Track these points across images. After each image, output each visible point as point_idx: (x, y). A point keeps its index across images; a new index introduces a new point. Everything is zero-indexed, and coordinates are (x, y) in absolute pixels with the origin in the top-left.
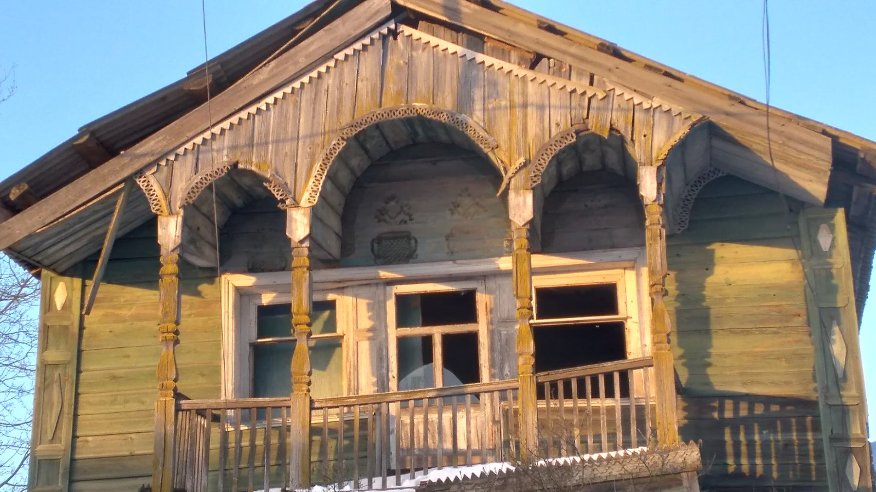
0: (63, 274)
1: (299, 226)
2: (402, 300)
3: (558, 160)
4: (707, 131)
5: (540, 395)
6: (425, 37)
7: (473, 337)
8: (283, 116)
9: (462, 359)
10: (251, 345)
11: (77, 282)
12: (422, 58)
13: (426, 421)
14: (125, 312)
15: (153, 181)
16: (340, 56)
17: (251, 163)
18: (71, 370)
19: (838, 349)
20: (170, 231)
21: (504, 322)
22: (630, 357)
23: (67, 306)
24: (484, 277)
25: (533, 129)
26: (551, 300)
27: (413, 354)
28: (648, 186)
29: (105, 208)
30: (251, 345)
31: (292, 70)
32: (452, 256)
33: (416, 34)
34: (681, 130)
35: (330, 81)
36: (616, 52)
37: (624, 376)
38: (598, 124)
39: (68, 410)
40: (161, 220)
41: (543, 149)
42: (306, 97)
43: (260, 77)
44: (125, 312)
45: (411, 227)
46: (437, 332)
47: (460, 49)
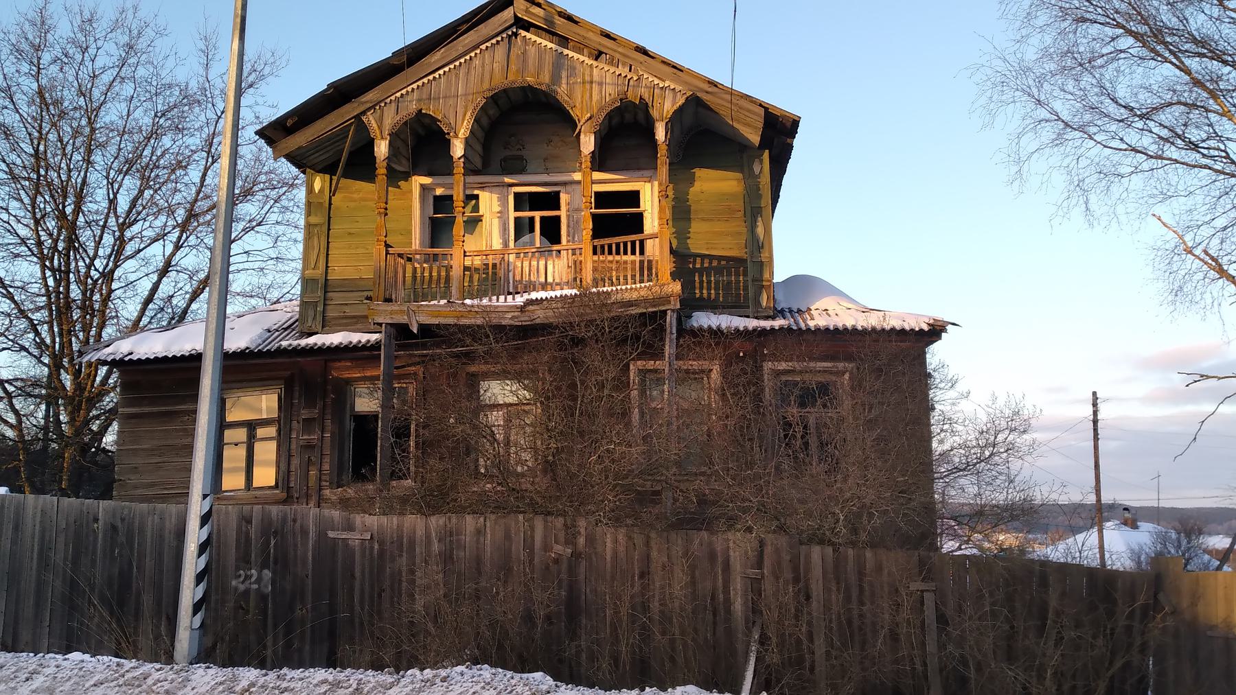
0: (319, 172)
2: (517, 195)
3: (609, 116)
5: (595, 253)
7: (558, 218)
9: (551, 231)
11: (327, 177)
12: (532, 50)
14: (355, 196)
19: (760, 230)
20: (382, 149)
21: (576, 209)
24: (565, 184)
25: (595, 97)
26: (603, 199)
27: (523, 227)
28: (660, 134)
31: (455, 55)
32: (547, 171)
33: (528, 35)
34: (681, 101)
35: (477, 62)
36: (644, 51)
39: (323, 251)
41: (601, 109)
43: (436, 57)
44: (355, 196)
45: (523, 153)
46: (537, 215)
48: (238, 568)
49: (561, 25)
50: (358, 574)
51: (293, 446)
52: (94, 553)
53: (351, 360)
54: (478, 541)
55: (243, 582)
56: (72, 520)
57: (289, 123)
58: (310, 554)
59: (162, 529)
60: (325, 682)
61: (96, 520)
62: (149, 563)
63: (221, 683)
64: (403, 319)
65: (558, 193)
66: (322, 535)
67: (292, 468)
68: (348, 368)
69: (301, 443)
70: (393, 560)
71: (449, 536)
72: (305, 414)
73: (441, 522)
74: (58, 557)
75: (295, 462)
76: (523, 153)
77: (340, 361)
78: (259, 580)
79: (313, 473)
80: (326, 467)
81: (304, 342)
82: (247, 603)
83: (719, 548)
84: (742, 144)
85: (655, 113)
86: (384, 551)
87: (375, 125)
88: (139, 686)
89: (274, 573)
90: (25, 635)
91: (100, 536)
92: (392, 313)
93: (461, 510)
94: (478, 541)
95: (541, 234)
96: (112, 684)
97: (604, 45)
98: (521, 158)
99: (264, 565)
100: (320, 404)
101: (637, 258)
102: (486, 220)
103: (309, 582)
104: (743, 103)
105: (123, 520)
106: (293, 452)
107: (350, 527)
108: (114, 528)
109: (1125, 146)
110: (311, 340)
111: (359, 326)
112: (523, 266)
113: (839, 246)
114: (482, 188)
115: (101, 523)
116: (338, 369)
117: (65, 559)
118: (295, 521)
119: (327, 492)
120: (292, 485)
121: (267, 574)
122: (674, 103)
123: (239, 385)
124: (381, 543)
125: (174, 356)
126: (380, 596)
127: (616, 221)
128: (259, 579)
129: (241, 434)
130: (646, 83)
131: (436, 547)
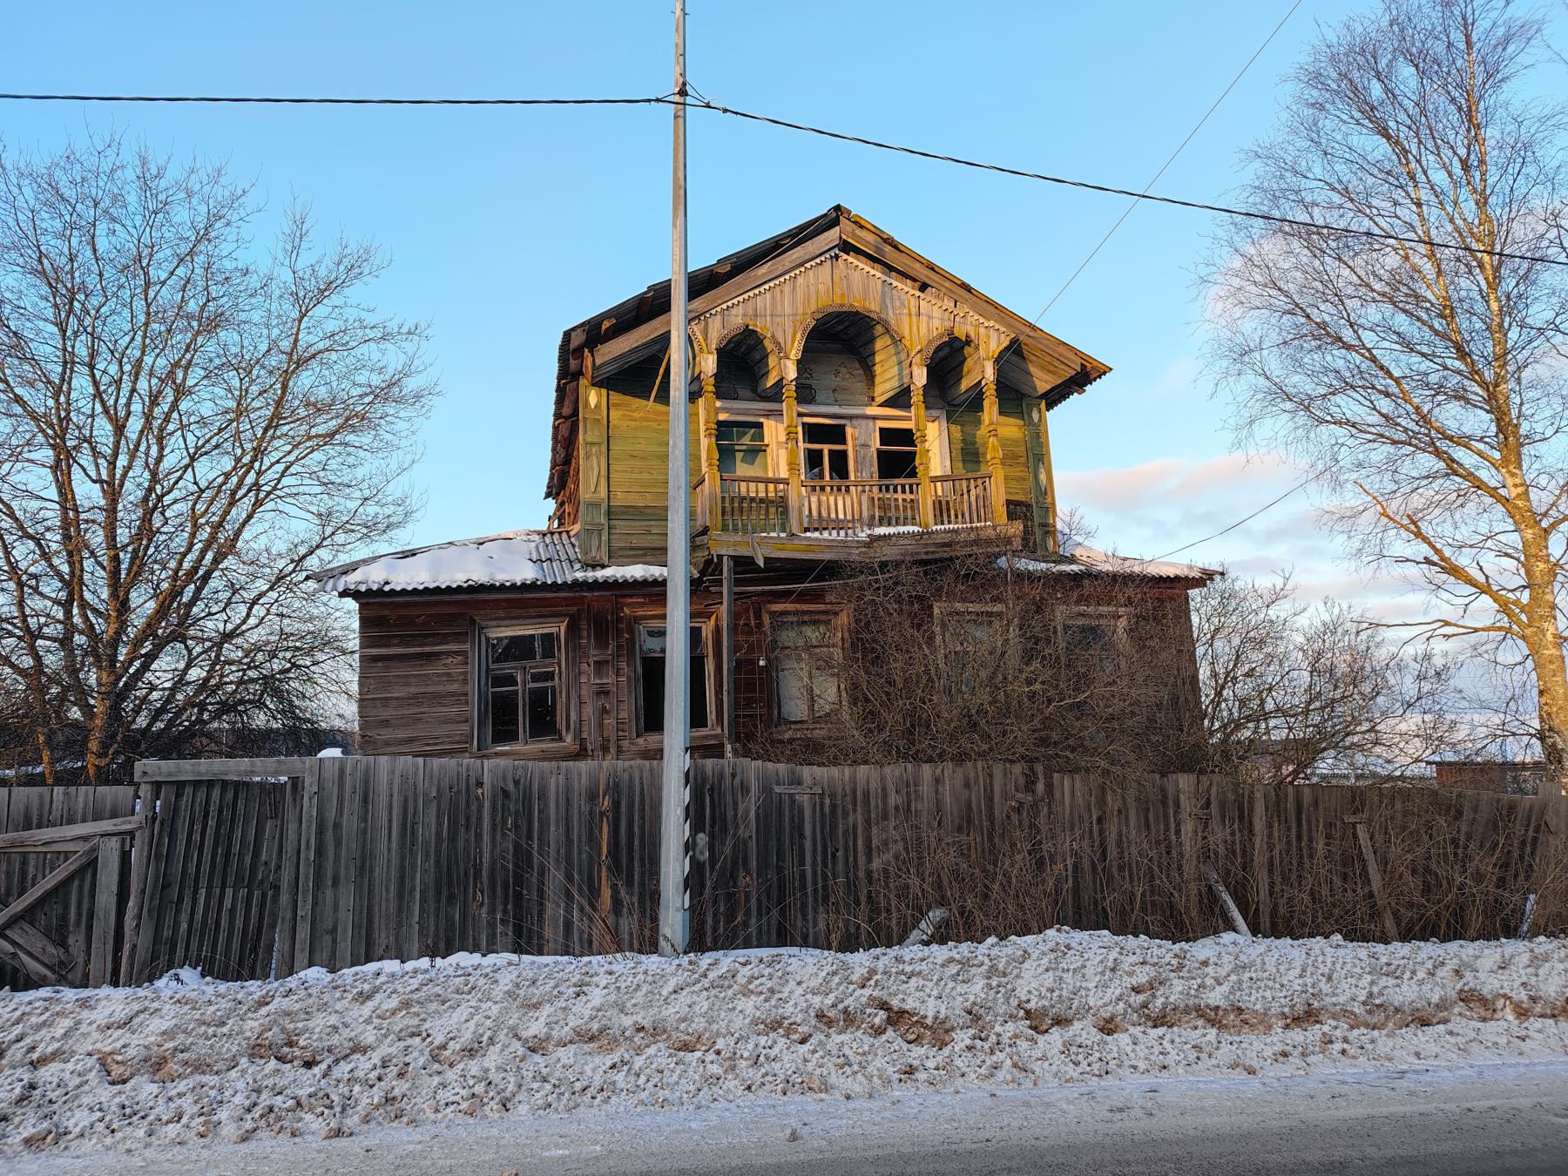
3: (938, 349)
7: (844, 453)
8: (773, 297)
9: (840, 465)
11: (604, 392)
12: (856, 275)
13: (819, 502)
14: (636, 415)
17: (758, 326)
18: (604, 448)
19: (1043, 477)
21: (862, 442)
23: (598, 406)
24: (851, 418)
25: (923, 330)
26: (887, 436)
27: (814, 459)
32: (836, 402)
33: (850, 259)
35: (800, 280)
36: (967, 288)
38: (960, 332)
42: (787, 288)
43: (763, 271)
44: (636, 415)
46: (826, 448)
47: (879, 274)
49: (890, 255)
50: (808, 832)
53: (644, 596)
54: (937, 792)
56: (445, 785)
57: (606, 324)
58: (752, 813)
59: (568, 790)
60: (951, 960)
61: (480, 784)
63: (835, 973)
64: (744, 551)
65: (843, 427)
66: (766, 790)
68: (641, 605)
70: (845, 815)
71: (909, 788)
73: (897, 773)
74: (427, 828)
77: (631, 596)
81: (591, 575)
83: (1171, 789)
86: (832, 808)
88: (730, 987)
89: (712, 836)
90: (382, 938)
91: (487, 805)
92: (735, 544)
94: (937, 792)
96: (698, 987)
100: (612, 645)
102: (773, 446)
104: (1061, 349)
105: (517, 783)
106: (585, 699)
107: (796, 781)
108: (506, 793)
110: (600, 574)
111: (648, 559)
112: (799, 496)
114: (767, 416)
118: (734, 775)
120: (584, 735)
124: (833, 796)
125: (404, 590)
126: (834, 856)
127: (898, 458)
130: (969, 323)
131: (893, 799)
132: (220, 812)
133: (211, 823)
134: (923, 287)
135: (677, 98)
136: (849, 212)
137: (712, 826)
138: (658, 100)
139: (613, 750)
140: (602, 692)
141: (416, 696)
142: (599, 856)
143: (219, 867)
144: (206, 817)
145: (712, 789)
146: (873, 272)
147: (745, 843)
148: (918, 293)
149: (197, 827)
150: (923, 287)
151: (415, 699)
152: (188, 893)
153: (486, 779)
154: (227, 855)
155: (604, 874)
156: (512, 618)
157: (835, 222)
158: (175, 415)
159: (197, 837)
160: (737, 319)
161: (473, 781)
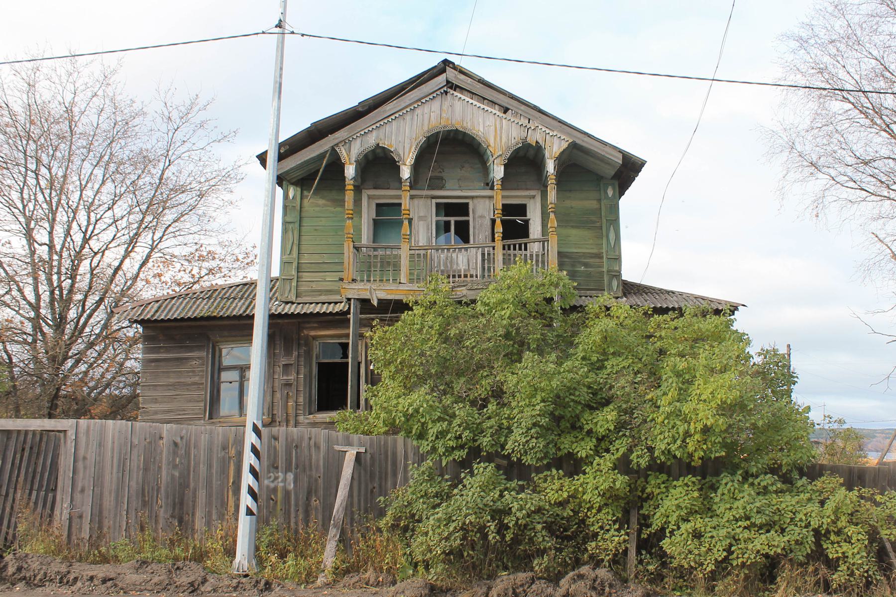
0: (292, 184)
1: (406, 173)
2: (437, 205)
4: (574, 146)
5: (504, 249)
6: (459, 95)
7: (468, 221)
9: (463, 232)
10: (374, 220)
15: (342, 149)
16: (424, 101)
17: (385, 144)
18: (297, 225)
20: (350, 171)
21: (484, 211)
22: (531, 236)
24: (472, 197)
25: (504, 140)
28: (550, 167)
29: (322, 156)
30: (374, 220)
31: (403, 105)
33: (456, 93)
34: (565, 145)
37: (526, 245)
38: (531, 140)
39: (296, 242)
40: (346, 167)
41: (508, 148)
43: (389, 108)
45: (443, 174)
46: (453, 220)
48: (269, 472)
51: (276, 384)
52: (161, 462)
55: (273, 482)
61: (161, 438)
62: (203, 468)
64: (366, 295)
65: (467, 204)
66: (329, 448)
67: (275, 401)
68: (314, 329)
69: (283, 382)
72: (284, 361)
75: (278, 395)
76: (443, 174)
78: (285, 480)
79: (291, 403)
80: (301, 399)
82: (276, 496)
84: (598, 175)
85: (547, 154)
87: (345, 154)
93: (92, 418)
95: (456, 233)
97: (506, 103)
98: (442, 179)
99: (288, 469)
100: (295, 353)
101: (524, 252)
103: (320, 481)
105: (182, 438)
108: (176, 444)
109: (856, 186)
113: (655, 243)
115: (165, 440)
116: (306, 328)
117: (139, 467)
118: (310, 439)
119: (301, 418)
121: (290, 476)
122: (560, 147)
123: (239, 338)
128: (286, 481)
129: (234, 375)
132: (31, 448)
133: (26, 454)
134: (506, 110)
135: (278, 30)
136: (453, 64)
137: (296, 468)
138: (263, 33)
139: (292, 422)
140: (288, 385)
141: (173, 385)
142: (228, 482)
143: (30, 479)
144: (23, 450)
145: (297, 446)
146: (471, 101)
147: (316, 480)
148: (501, 115)
149: (18, 456)
150: (506, 110)
151: (174, 386)
152: (11, 491)
153: (164, 435)
154: (35, 472)
155: (230, 493)
156: (243, 336)
157: (443, 71)
158: (81, 202)
159: (17, 461)
160: (371, 141)
161: (158, 436)
